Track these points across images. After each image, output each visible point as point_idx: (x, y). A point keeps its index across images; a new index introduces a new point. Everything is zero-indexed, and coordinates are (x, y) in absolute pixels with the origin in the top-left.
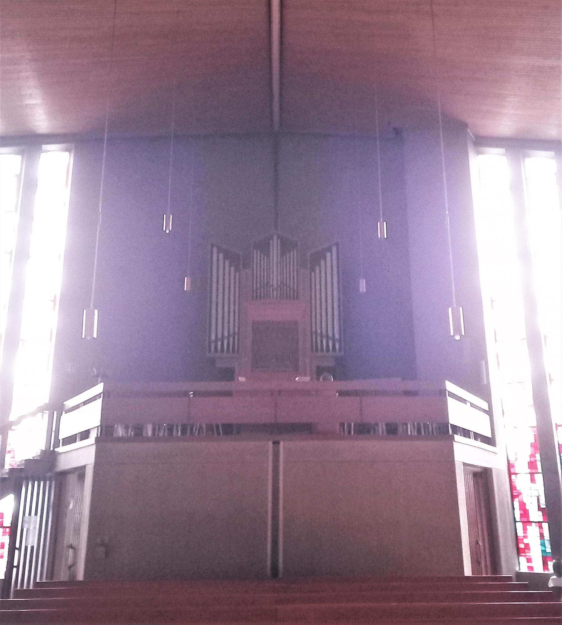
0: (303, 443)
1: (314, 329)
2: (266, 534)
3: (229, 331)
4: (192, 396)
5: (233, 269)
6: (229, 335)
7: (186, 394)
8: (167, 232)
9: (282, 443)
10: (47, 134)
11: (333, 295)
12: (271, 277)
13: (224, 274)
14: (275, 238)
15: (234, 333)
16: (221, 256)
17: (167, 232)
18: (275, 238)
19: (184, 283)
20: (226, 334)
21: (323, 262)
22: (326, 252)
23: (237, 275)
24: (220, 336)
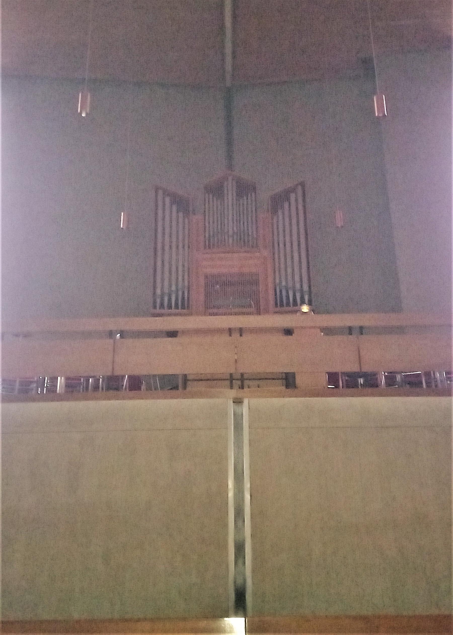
0: (277, 402)
1: (277, 281)
2: (158, 386)
3: (177, 285)
4: (119, 335)
5: (181, 215)
6: (177, 290)
7: (111, 334)
8: (84, 115)
9: (246, 401)
10: (252, 562)
11: (299, 242)
12: (226, 222)
13: (171, 227)
14: (230, 178)
15: (184, 287)
16: (167, 200)
17: (84, 115)
18: (230, 178)
19: (123, 223)
20: (174, 288)
21: (286, 205)
22: (289, 194)
23: (186, 220)
24: (166, 291)
